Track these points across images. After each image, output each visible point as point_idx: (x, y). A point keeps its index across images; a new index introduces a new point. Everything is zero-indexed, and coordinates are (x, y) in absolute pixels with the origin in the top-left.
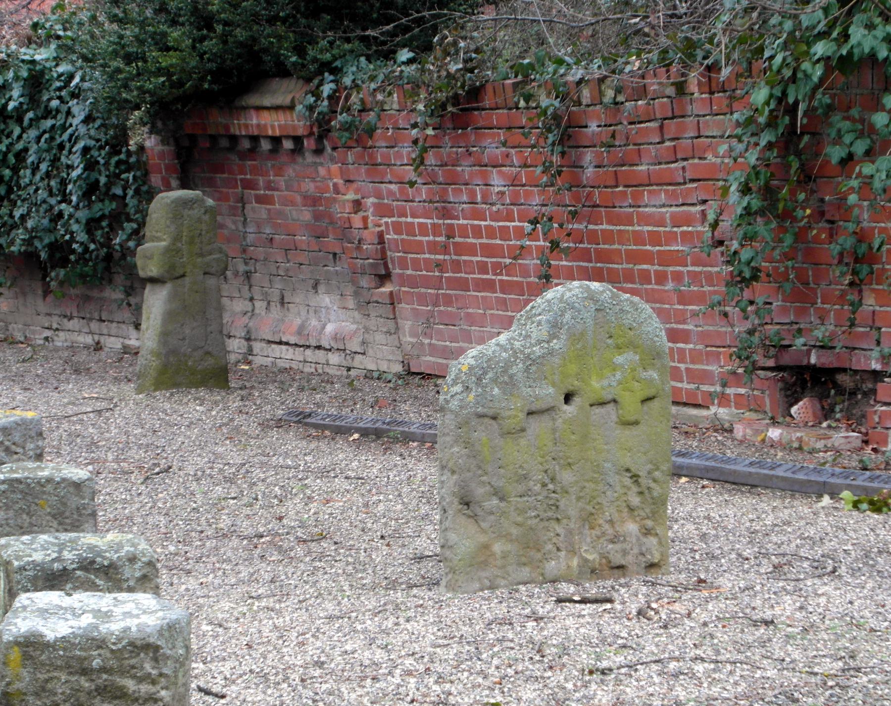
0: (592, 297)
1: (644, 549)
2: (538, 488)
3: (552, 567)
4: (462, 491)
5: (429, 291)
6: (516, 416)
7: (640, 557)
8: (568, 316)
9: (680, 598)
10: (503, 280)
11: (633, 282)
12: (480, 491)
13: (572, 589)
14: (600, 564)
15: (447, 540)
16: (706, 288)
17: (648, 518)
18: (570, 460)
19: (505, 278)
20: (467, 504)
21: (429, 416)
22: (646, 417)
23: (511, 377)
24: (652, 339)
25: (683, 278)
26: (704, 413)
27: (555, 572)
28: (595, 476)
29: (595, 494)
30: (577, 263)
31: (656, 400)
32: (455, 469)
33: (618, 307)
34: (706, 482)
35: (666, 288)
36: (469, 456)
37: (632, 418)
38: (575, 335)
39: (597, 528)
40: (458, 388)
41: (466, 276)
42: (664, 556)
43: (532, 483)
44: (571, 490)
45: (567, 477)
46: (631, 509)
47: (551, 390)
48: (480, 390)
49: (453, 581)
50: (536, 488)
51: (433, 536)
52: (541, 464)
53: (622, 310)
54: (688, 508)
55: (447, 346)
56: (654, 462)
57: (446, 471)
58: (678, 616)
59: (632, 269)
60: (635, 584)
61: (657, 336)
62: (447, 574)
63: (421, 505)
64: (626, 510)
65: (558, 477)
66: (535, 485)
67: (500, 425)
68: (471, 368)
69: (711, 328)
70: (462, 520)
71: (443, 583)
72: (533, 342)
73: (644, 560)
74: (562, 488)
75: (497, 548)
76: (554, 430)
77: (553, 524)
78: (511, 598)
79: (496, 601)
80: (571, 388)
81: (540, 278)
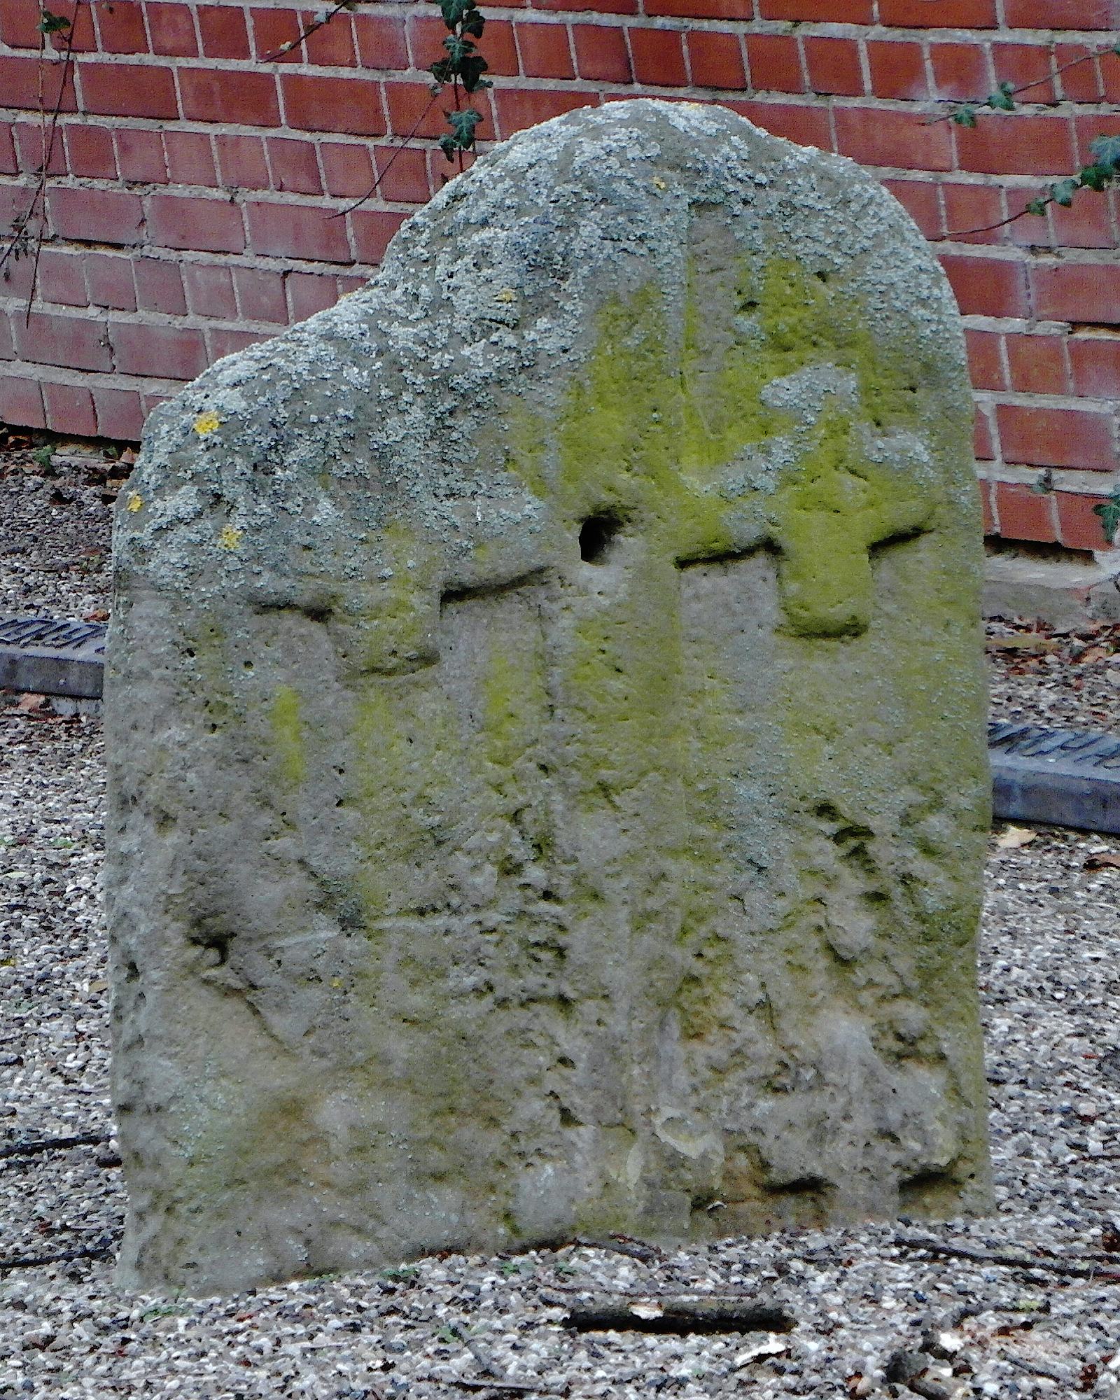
0: (678, 159)
1: (894, 1116)
2: (485, 879)
3: (544, 1189)
4: (201, 892)
5: (23, 117)
6: (400, 605)
7: (880, 1147)
8: (589, 229)
9: (1046, 1309)
10: (299, 78)
11: (791, 87)
12: (264, 895)
13: (626, 1273)
14: (728, 1176)
15: (142, 1084)
16: (1070, 110)
17: (907, 993)
18: (605, 774)
19: (306, 69)
20: (220, 943)
21: (28, 590)
22: (890, 607)
23: (381, 456)
24: (904, 313)
25: (980, 70)
26: (1072, 575)
27: (557, 1205)
28: (702, 831)
29: (704, 900)
30: (581, 17)
31: (923, 541)
32: (173, 808)
33: (775, 195)
34: (1099, 847)
35: (917, 108)
36: (223, 761)
37: (838, 613)
38: (617, 301)
39: (714, 1034)
40: (183, 501)
41: (163, 62)
42: (971, 1140)
43: (463, 861)
44: (612, 888)
45: (593, 836)
46: (842, 961)
47: (531, 506)
48: (264, 507)
49: (166, 1246)
50: (478, 880)
51: (72, 1062)
52: (498, 788)
53: (789, 208)
54: (1043, 950)
55: (89, 324)
56: (925, 777)
57: (136, 817)
58: (1042, 1382)
59: (788, 40)
60: (867, 1255)
61: (923, 302)
62: (140, 1215)
63: (18, 938)
64: (824, 962)
65: (562, 839)
66: (476, 868)
67: (339, 639)
68: (230, 424)
69: (1090, 258)
70: (202, 1004)
71: (125, 1254)
72: (461, 325)
73: (895, 1156)
74: (577, 880)
75: (334, 1112)
76: (545, 660)
77: (547, 1018)
78: (393, 1311)
79: (335, 1322)
80: (607, 498)
81: (442, 70)
